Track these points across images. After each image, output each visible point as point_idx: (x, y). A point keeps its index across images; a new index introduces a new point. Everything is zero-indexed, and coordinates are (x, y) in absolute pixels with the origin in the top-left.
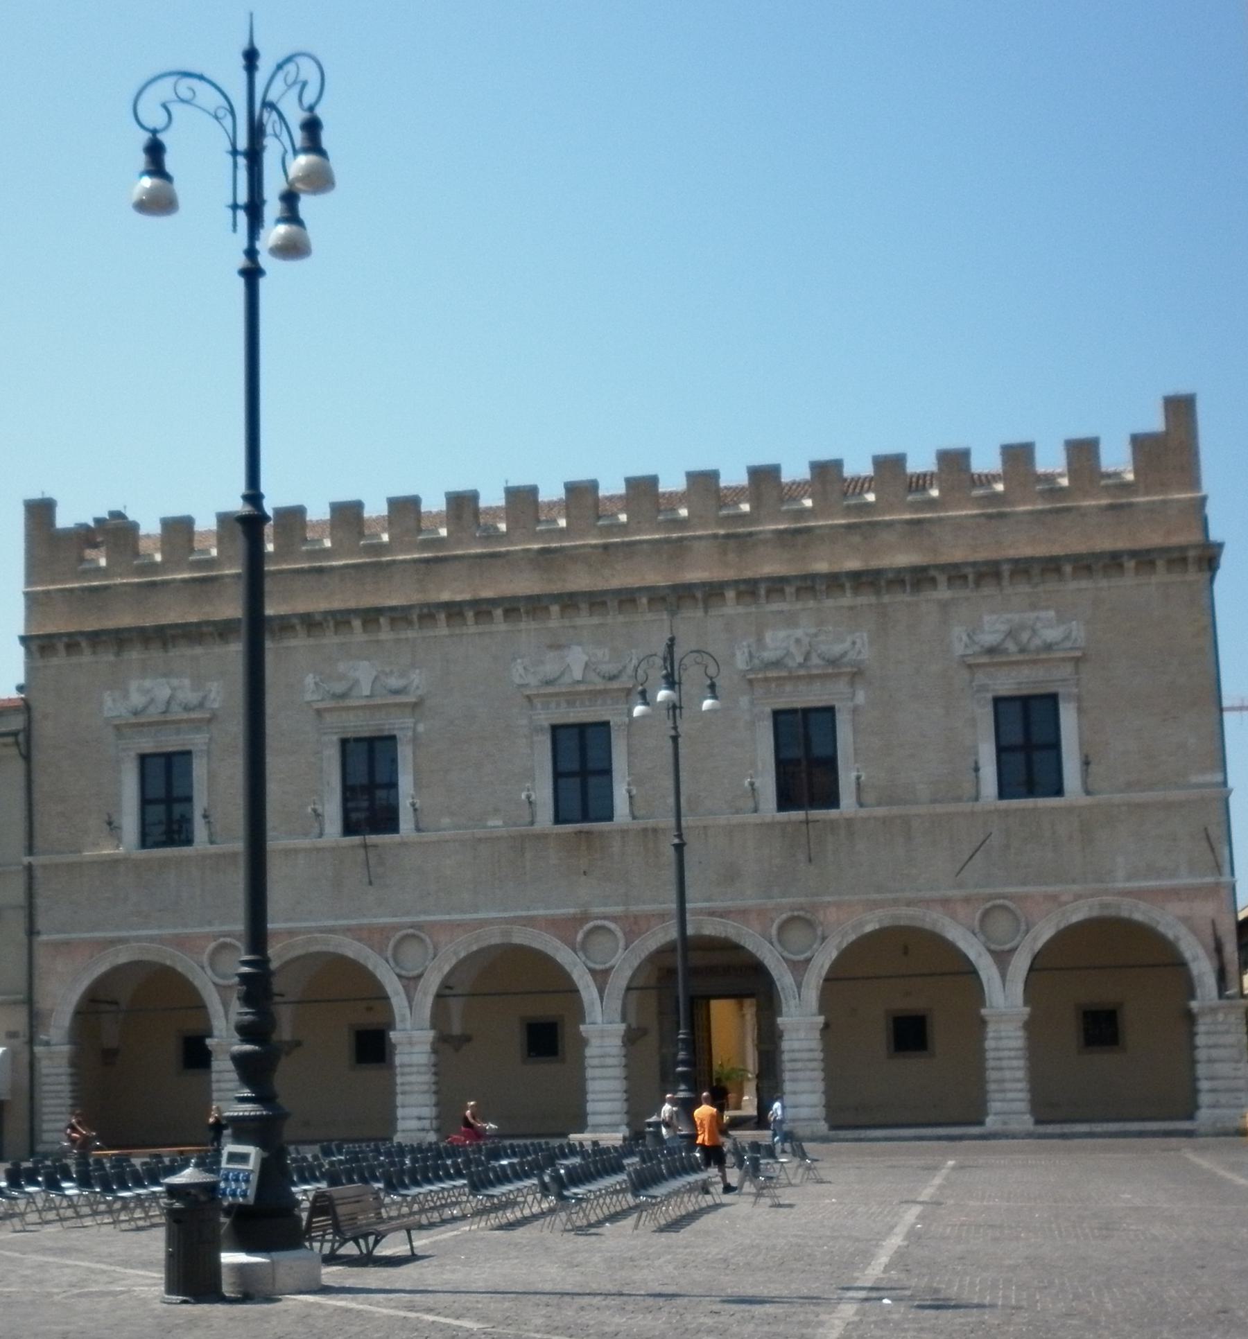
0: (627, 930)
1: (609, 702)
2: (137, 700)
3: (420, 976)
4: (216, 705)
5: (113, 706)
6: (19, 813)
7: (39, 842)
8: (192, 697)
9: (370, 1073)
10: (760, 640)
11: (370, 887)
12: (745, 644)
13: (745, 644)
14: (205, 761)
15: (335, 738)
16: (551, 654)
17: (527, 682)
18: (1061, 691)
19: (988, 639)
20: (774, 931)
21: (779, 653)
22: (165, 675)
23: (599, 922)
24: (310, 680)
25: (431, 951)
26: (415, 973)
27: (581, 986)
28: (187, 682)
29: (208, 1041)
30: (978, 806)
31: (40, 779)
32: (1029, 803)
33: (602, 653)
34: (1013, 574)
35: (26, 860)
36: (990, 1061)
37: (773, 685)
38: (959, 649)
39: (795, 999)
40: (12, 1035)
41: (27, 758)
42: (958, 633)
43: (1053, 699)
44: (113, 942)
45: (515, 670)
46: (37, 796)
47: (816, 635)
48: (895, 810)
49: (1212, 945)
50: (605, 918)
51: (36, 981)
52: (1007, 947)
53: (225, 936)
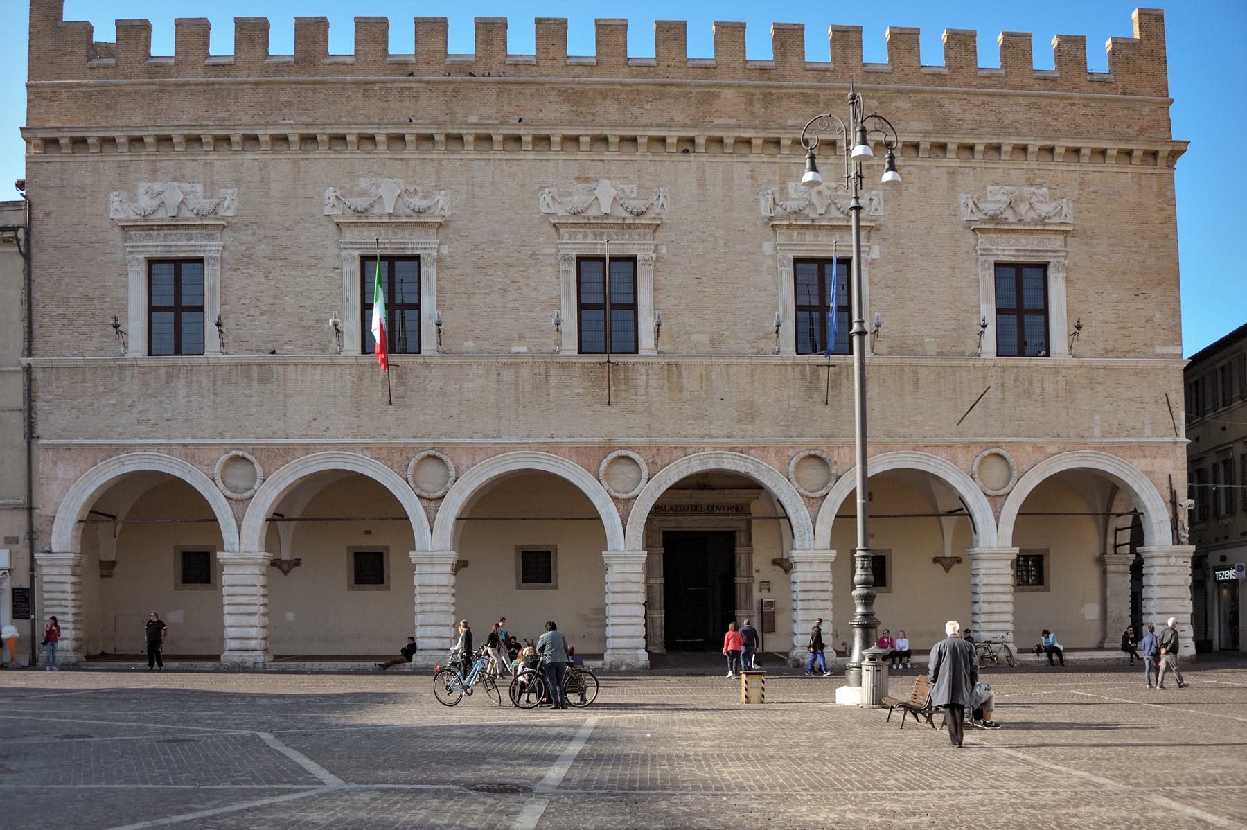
0: (650, 461)
1: (636, 237)
2: (146, 202)
3: (442, 497)
4: (229, 213)
5: (120, 208)
6: (17, 313)
7: (38, 343)
8: (206, 205)
9: (196, 594)
10: (783, 190)
11: (390, 406)
12: (769, 191)
13: (769, 191)
14: (218, 267)
15: (356, 254)
16: (580, 186)
17: (553, 212)
18: (1053, 260)
19: (990, 208)
20: (792, 469)
21: (803, 203)
22: (175, 179)
23: (623, 453)
24: (330, 193)
25: (452, 474)
26: (440, 493)
27: (603, 514)
28: (199, 188)
29: (219, 555)
30: (979, 363)
31: (39, 278)
32: (1024, 361)
33: (631, 189)
34: (985, 153)
35: (25, 361)
36: (610, 595)
37: (795, 234)
38: (965, 215)
39: (809, 533)
40: (11, 541)
41: (27, 256)
42: (965, 200)
43: (1044, 267)
44: (118, 449)
45: (542, 199)
46: (36, 296)
47: (836, 189)
48: (907, 361)
49: (1169, 498)
50: (629, 448)
51: (36, 489)
52: (1001, 492)
53: (238, 449)
